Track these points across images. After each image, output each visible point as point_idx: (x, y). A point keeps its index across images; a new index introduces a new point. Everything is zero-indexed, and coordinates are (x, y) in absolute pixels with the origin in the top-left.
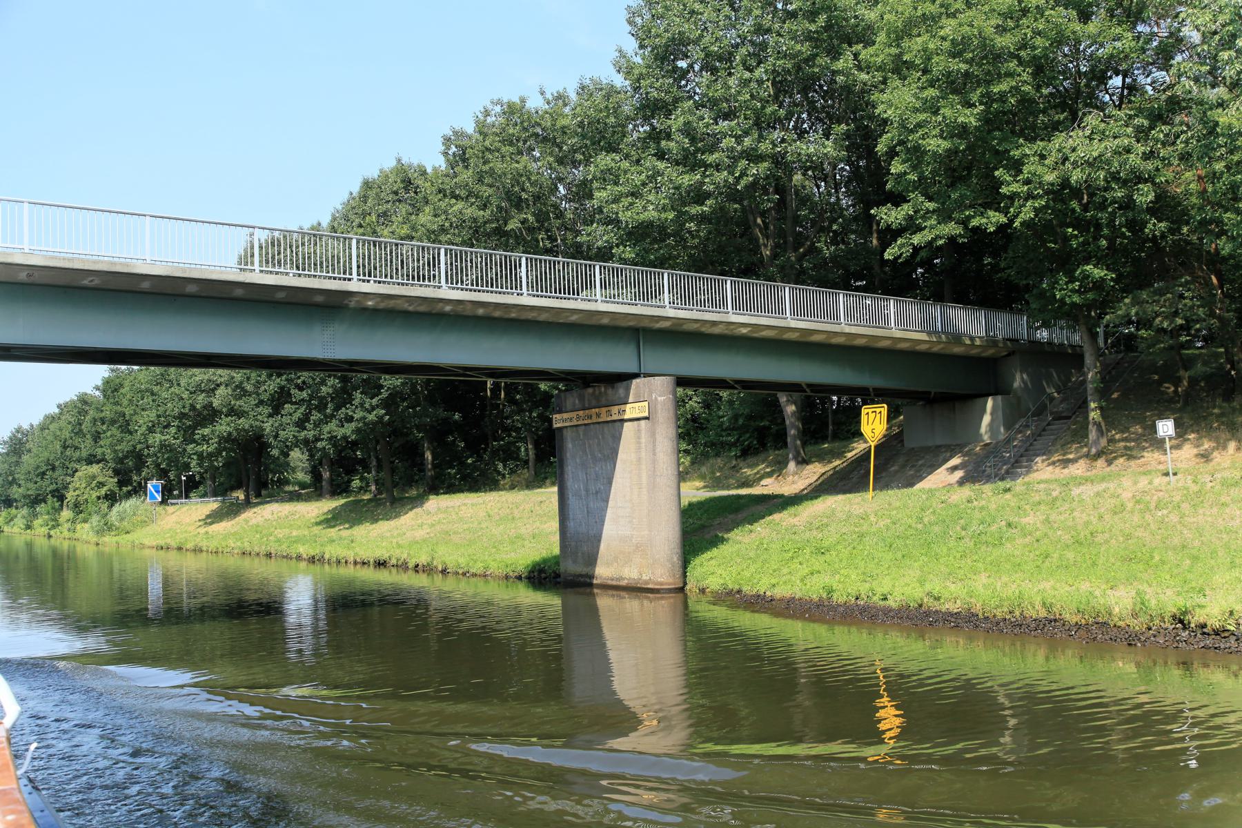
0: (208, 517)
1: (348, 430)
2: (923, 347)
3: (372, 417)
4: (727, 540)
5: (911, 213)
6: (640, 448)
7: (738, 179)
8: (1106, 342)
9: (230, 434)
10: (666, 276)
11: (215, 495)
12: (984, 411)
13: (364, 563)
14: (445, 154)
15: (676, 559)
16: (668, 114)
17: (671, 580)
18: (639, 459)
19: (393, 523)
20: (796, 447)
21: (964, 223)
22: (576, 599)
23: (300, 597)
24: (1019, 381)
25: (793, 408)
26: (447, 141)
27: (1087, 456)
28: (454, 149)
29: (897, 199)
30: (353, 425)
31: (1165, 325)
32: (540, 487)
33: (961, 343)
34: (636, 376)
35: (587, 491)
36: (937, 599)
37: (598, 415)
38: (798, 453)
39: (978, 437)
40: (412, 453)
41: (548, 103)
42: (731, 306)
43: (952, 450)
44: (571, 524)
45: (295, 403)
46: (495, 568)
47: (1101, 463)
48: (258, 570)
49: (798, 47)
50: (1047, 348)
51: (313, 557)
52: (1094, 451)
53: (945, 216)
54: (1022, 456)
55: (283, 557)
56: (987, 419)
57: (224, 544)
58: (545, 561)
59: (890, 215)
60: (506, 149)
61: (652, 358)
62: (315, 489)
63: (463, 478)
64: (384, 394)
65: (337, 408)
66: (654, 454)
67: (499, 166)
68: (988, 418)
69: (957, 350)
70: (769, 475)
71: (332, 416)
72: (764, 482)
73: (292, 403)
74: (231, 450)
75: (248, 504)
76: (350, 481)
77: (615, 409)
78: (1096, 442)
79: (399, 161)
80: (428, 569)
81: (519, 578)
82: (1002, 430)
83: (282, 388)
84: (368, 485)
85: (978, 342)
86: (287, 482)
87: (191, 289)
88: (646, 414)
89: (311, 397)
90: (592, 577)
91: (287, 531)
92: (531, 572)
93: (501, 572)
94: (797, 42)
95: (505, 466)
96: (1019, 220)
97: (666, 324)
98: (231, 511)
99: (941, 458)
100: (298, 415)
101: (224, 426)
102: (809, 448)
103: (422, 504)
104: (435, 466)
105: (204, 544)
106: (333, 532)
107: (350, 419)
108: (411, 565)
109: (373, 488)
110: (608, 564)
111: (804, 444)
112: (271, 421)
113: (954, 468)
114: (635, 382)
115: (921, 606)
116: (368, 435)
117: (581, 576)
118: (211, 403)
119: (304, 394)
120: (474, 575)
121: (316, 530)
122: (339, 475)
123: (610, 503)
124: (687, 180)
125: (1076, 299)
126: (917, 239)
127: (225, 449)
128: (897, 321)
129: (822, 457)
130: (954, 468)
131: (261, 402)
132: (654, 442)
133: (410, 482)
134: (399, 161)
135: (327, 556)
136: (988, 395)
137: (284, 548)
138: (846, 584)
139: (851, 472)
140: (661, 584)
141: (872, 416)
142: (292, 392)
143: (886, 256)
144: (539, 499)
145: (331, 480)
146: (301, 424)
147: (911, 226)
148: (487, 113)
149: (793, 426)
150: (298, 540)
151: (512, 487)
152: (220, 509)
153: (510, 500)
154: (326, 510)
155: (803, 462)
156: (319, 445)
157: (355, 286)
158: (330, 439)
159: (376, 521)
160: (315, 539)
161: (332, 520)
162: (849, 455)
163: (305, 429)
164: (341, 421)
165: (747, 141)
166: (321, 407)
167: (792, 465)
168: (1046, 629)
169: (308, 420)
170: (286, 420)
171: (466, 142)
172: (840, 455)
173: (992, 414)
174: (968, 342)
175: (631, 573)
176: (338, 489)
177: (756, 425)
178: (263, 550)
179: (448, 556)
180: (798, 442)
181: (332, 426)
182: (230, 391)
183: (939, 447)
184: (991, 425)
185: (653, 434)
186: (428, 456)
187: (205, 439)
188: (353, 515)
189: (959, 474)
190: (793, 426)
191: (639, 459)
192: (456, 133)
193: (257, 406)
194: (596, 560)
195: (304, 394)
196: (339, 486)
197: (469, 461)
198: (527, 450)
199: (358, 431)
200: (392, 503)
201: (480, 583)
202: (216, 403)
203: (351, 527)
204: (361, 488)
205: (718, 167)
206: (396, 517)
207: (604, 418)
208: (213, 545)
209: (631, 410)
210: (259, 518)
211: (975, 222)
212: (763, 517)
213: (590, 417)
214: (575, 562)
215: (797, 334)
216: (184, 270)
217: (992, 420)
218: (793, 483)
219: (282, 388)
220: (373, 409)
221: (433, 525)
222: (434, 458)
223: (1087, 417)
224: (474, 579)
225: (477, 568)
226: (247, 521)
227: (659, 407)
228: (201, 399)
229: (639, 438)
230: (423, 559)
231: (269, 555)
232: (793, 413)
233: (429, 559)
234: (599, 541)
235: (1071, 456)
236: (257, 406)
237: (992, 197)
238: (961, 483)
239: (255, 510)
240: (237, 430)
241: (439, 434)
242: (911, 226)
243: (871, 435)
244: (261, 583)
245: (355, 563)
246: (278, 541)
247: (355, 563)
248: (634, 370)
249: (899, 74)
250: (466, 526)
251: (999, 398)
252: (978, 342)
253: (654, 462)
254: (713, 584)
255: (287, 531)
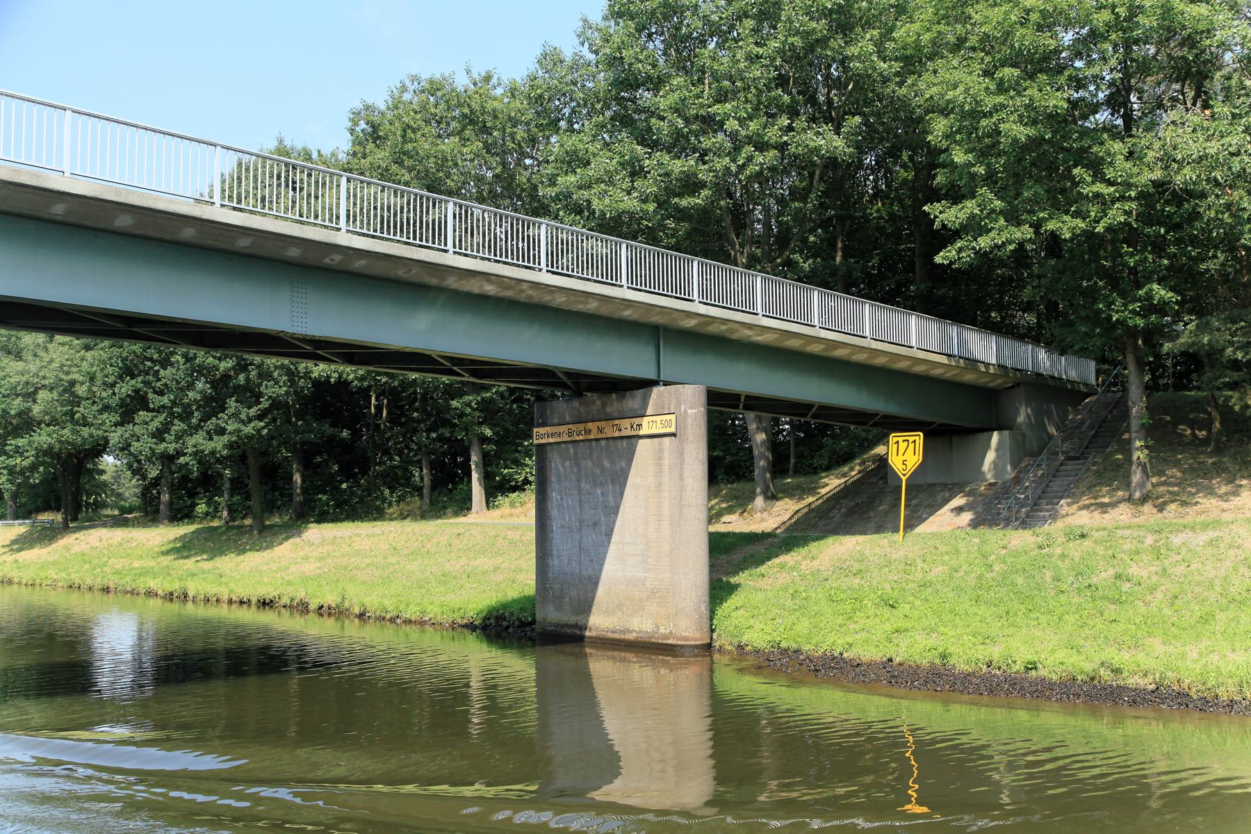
0: (14, 542)
1: (219, 443)
2: (937, 372)
3: (248, 430)
4: (736, 587)
5: (977, 211)
6: (661, 471)
7: (742, 168)
8: (1097, 379)
9: (51, 447)
10: (695, 264)
11: (16, 517)
12: (988, 446)
13: (242, 602)
14: (352, 131)
15: (704, 608)
16: (656, 89)
17: (698, 635)
18: (660, 484)
19: (266, 555)
20: (765, 480)
21: (1036, 226)
22: (557, 659)
23: (118, 640)
24: (1023, 415)
25: (763, 436)
26: (355, 117)
27: (1129, 500)
28: (363, 125)
29: (955, 195)
30: (225, 439)
31: (1239, 355)
32: (439, 517)
33: (977, 370)
34: (654, 383)
35: (581, 522)
36: (1117, 671)
37: (600, 430)
38: (767, 487)
39: (980, 476)
40: (274, 477)
41: (475, 84)
42: (761, 303)
43: (953, 489)
44: (554, 563)
45: (153, 410)
46: (433, 611)
47: (1148, 508)
48: (76, 606)
49: (814, 24)
50: (1051, 382)
51: (171, 594)
52: (1137, 495)
53: (1013, 218)
54: (1039, 498)
55: (126, 592)
56: (990, 456)
57: (42, 574)
58: (505, 606)
59: (947, 214)
60: (433, 130)
61: (673, 362)
62: (149, 511)
63: (337, 506)
64: (265, 404)
65: (205, 418)
66: (682, 478)
67: (425, 146)
68: (992, 455)
69: (969, 377)
70: (730, 510)
71: (198, 428)
72: (726, 518)
73: (149, 410)
74: (50, 465)
75: (65, 529)
76: (194, 505)
77: (626, 423)
78: (1142, 485)
79: (281, 141)
80: (336, 612)
81: (471, 627)
82: (1009, 468)
83: (137, 391)
84: (216, 510)
85: (992, 371)
86: (104, 505)
87: (123, 222)
88: (672, 430)
89: (174, 403)
90: (584, 627)
91: (126, 562)
92: (485, 619)
93: (447, 618)
94: (812, 19)
95: (392, 493)
96: (1102, 224)
97: (691, 323)
98: (48, 535)
99: (939, 498)
100: (156, 424)
101: (43, 438)
102: (778, 482)
103: (299, 534)
104: (305, 490)
105: (15, 575)
106: (189, 564)
107: (221, 431)
108: (312, 607)
109: (225, 513)
110: (609, 612)
111: (773, 478)
112: (120, 430)
113: (959, 510)
114: (656, 391)
115: (1092, 679)
116: (240, 453)
117: (566, 625)
118: (30, 410)
119: (165, 400)
120: (408, 622)
121: (166, 560)
122: (180, 498)
123: (615, 538)
124: (678, 166)
125: (1140, 322)
126: (984, 242)
127: (42, 464)
128: (917, 338)
129: (790, 493)
130: (959, 510)
131: (106, 408)
132: (682, 463)
133: (271, 507)
134: (281, 141)
135: (191, 594)
136: (994, 430)
137: (127, 582)
138: (866, 641)
139: (830, 510)
140: (686, 639)
141: (903, 446)
142: (151, 396)
143: (938, 259)
144: (456, 531)
145: (171, 503)
146: (159, 435)
147: (974, 227)
148: (404, 89)
149: (762, 456)
150: (144, 573)
151: (403, 517)
152: (30, 533)
153: (417, 530)
154: (172, 537)
155: (772, 497)
156: (182, 460)
157: (343, 239)
158: (195, 454)
159: (244, 551)
160: (167, 572)
161: (184, 548)
162: (823, 491)
163: (164, 440)
164: (208, 433)
165: (753, 126)
166: (186, 416)
167: (759, 501)
168: (938, 680)
169: (167, 430)
170: (138, 430)
171: (376, 119)
172: (812, 491)
173: (997, 450)
174: (983, 369)
175: (641, 625)
176: (180, 514)
177: (795, 450)
178: (99, 583)
179: (359, 596)
180: (768, 475)
181: (199, 438)
182: (55, 395)
183: (931, 485)
184: (995, 464)
185: (681, 454)
186: (297, 478)
187: (18, 451)
188: (211, 544)
189: (967, 517)
190: (762, 456)
191: (660, 484)
192: (367, 108)
193: (101, 412)
194: (590, 607)
195: (165, 400)
196: (179, 510)
197: (344, 486)
198: (422, 475)
199: (230, 446)
200: (260, 532)
201: (413, 632)
202: (36, 410)
203: (212, 559)
204: (207, 514)
205: (719, 153)
206: (267, 548)
207: (609, 432)
208: (27, 577)
209: (648, 425)
210: (84, 546)
211: (1051, 226)
212: (769, 559)
213: (589, 432)
214: (559, 608)
215: (822, 346)
216: (118, 192)
217: (998, 457)
218: (762, 520)
219: (137, 391)
220: (250, 420)
221: (323, 558)
222: (303, 481)
223: (1130, 455)
224: (407, 628)
225: (412, 612)
226: (67, 549)
227: (690, 421)
228: (17, 404)
229: (660, 458)
230: (331, 599)
231: (106, 590)
232: (763, 442)
233: (339, 600)
234: (596, 584)
235: (1106, 500)
236: (101, 412)
237: (1064, 198)
238: (975, 524)
239: (77, 535)
240: (60, 442)
241: (306, 454)
242: (974, 227)
243: (901, 467)
244: (263, 642)
245: (230, 602)
246: (117, 573)
247: (230, 602)
248: (652, 375)
249: (883, 77)
250: (367, 561)
251: (1006, 433)
252: (992, 371)
253: (682, 488)
254: (758, 636)
255: (126, 562)
